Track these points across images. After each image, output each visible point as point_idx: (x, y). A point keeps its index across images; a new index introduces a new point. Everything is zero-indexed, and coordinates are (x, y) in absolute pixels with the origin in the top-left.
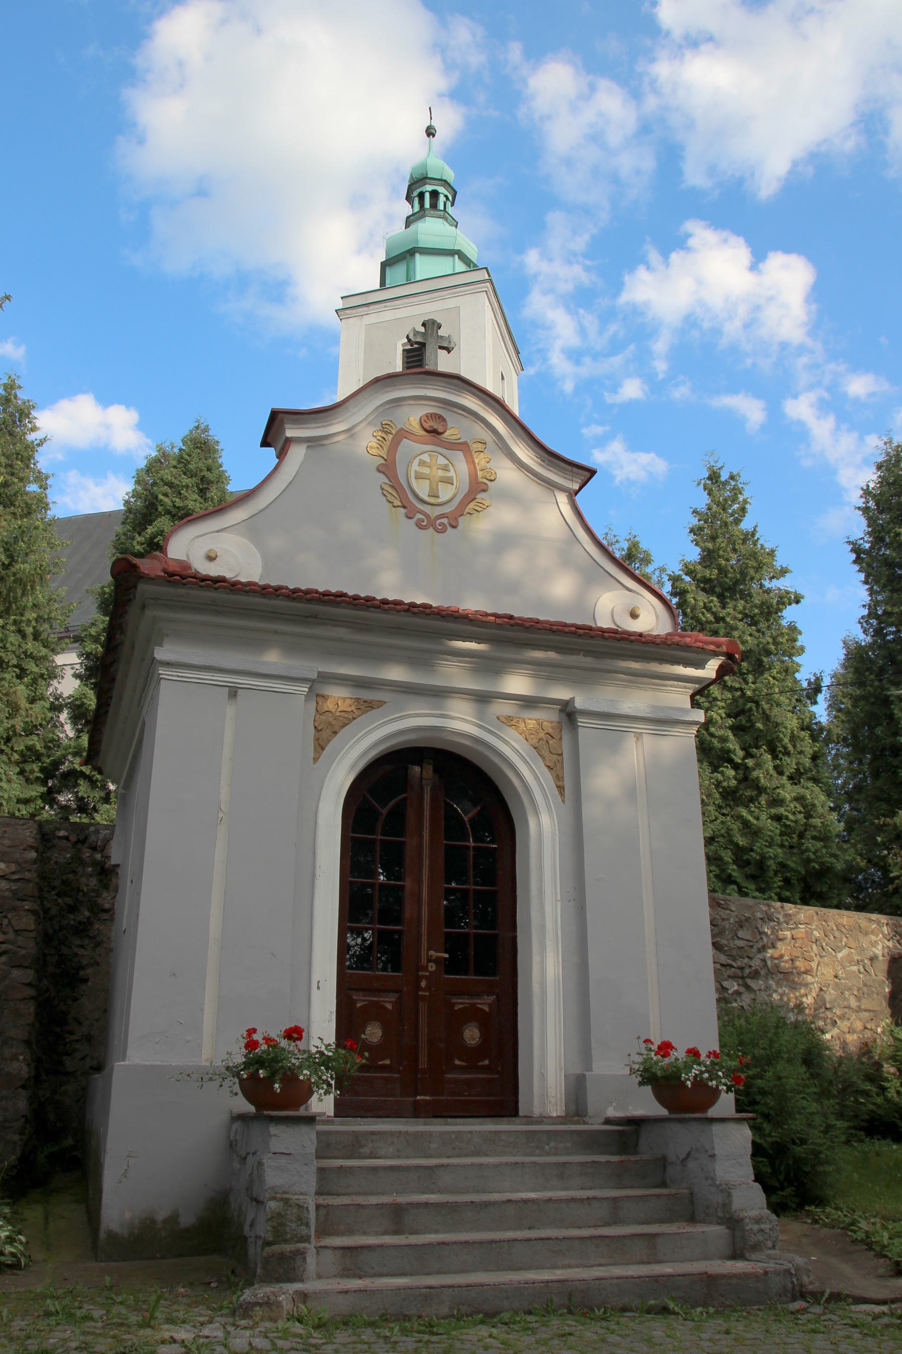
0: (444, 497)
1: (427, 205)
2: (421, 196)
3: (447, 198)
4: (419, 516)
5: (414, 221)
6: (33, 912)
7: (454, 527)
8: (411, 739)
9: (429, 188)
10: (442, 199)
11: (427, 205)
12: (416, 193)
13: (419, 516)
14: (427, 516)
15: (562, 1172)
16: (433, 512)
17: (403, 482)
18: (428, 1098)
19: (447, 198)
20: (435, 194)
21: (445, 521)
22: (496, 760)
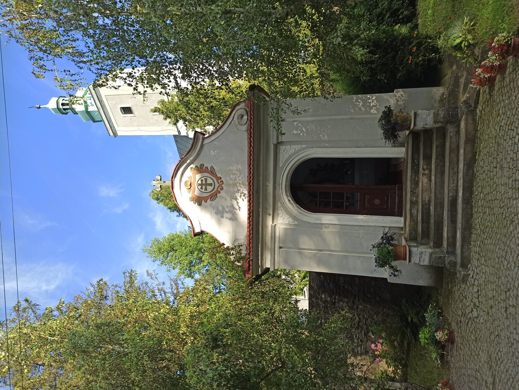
0: (211, 182)
1: (68, 107)
2: (64, 109)
3: (63, 100)
4: (219, 189)
5: (75, 112)
6: (362, 60)
7: (221, 178)
8: (288, 183)
9: (61, 107)
10: (64, 102)
11: (68, 107)
12: (64, 111)
13: (219, 189)
14: (219, 187)
15: (428, 158)
16: (217, 185)
17: (209, 194)
18: (396, 210)
19: (63, 100)
20: (63, 104)
21: (219, 181)
22: (295, 165)
